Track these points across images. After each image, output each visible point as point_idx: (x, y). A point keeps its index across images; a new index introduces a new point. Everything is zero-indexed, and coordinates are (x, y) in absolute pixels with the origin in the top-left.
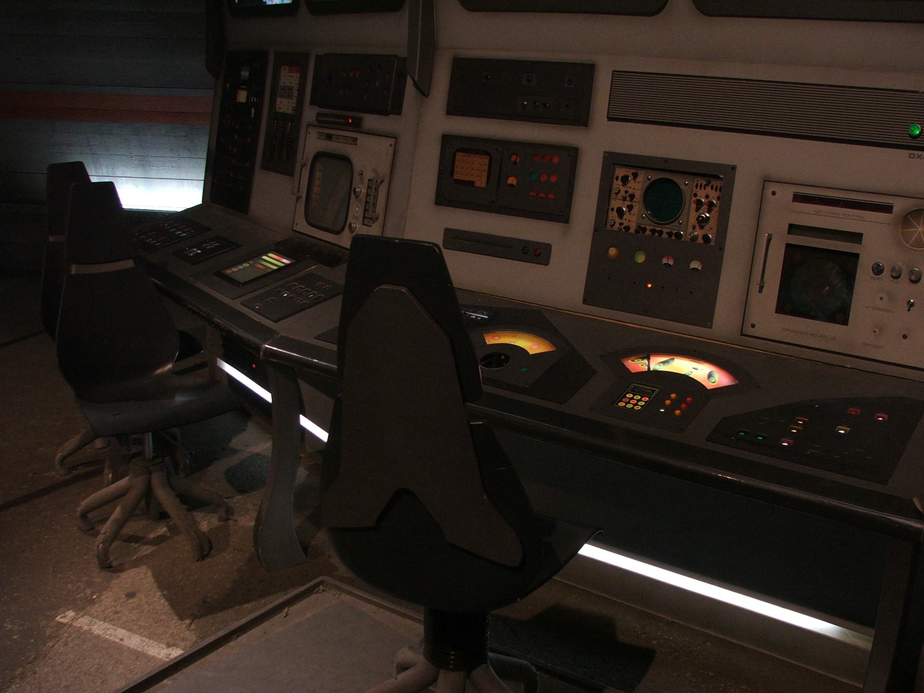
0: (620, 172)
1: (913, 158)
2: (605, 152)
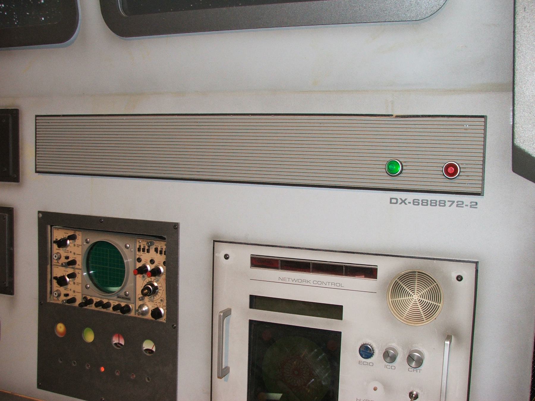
0: (59, 234)
1: (396, 203)
2: (39, 212)
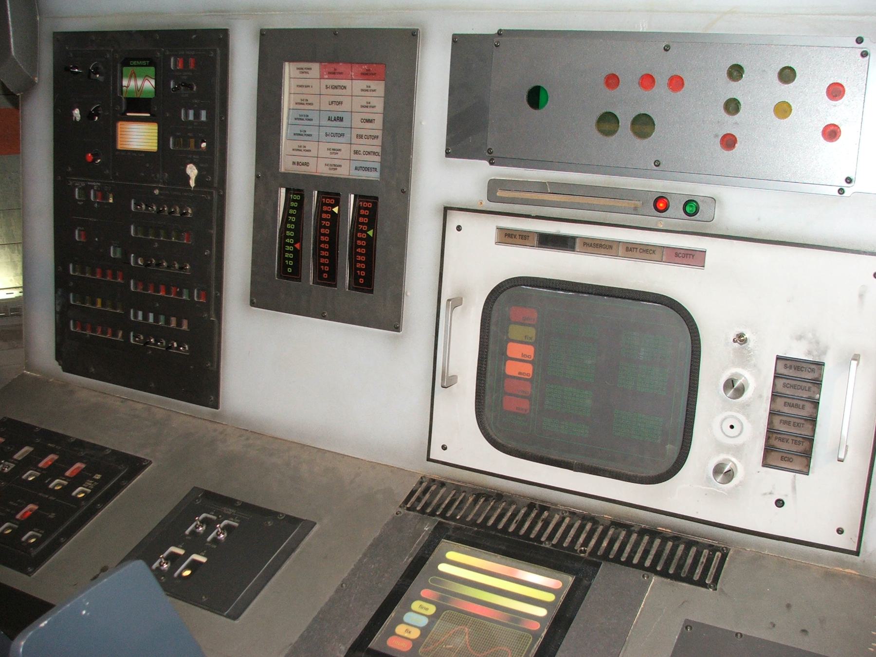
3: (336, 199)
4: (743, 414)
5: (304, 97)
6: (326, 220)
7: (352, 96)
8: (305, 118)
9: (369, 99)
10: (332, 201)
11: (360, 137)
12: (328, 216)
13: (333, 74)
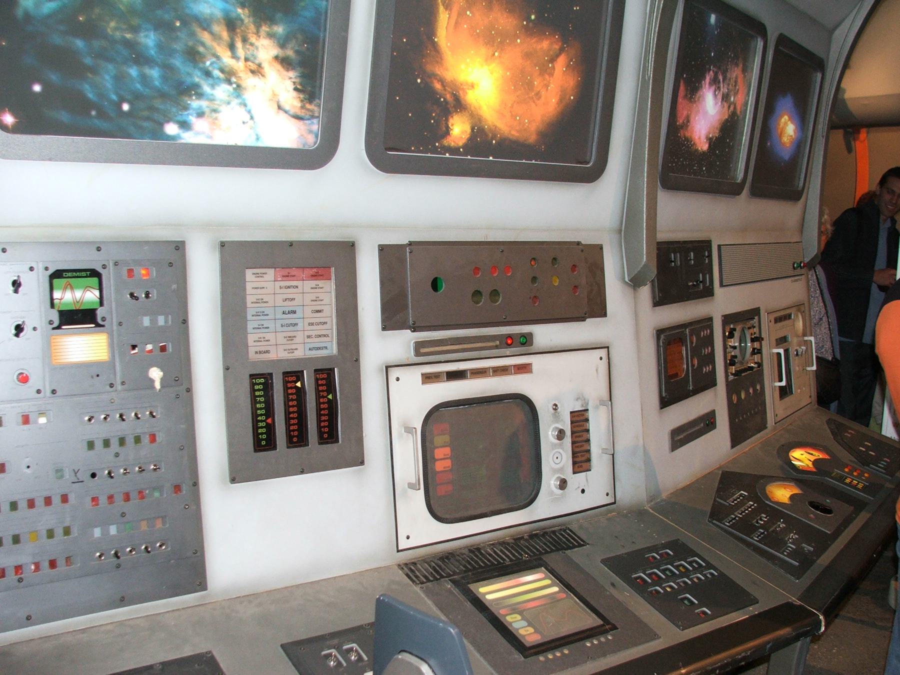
2: (252, 376)
3: (299, 375)
4: (561, 449)
5: (260, 297)
6: (292, 394)
7: (274, 294)
8: (261, 314)
9: (317, 295)
10: (294, 378)
11: (311, 324)
12: (294, 391)
13: (286, 277)
